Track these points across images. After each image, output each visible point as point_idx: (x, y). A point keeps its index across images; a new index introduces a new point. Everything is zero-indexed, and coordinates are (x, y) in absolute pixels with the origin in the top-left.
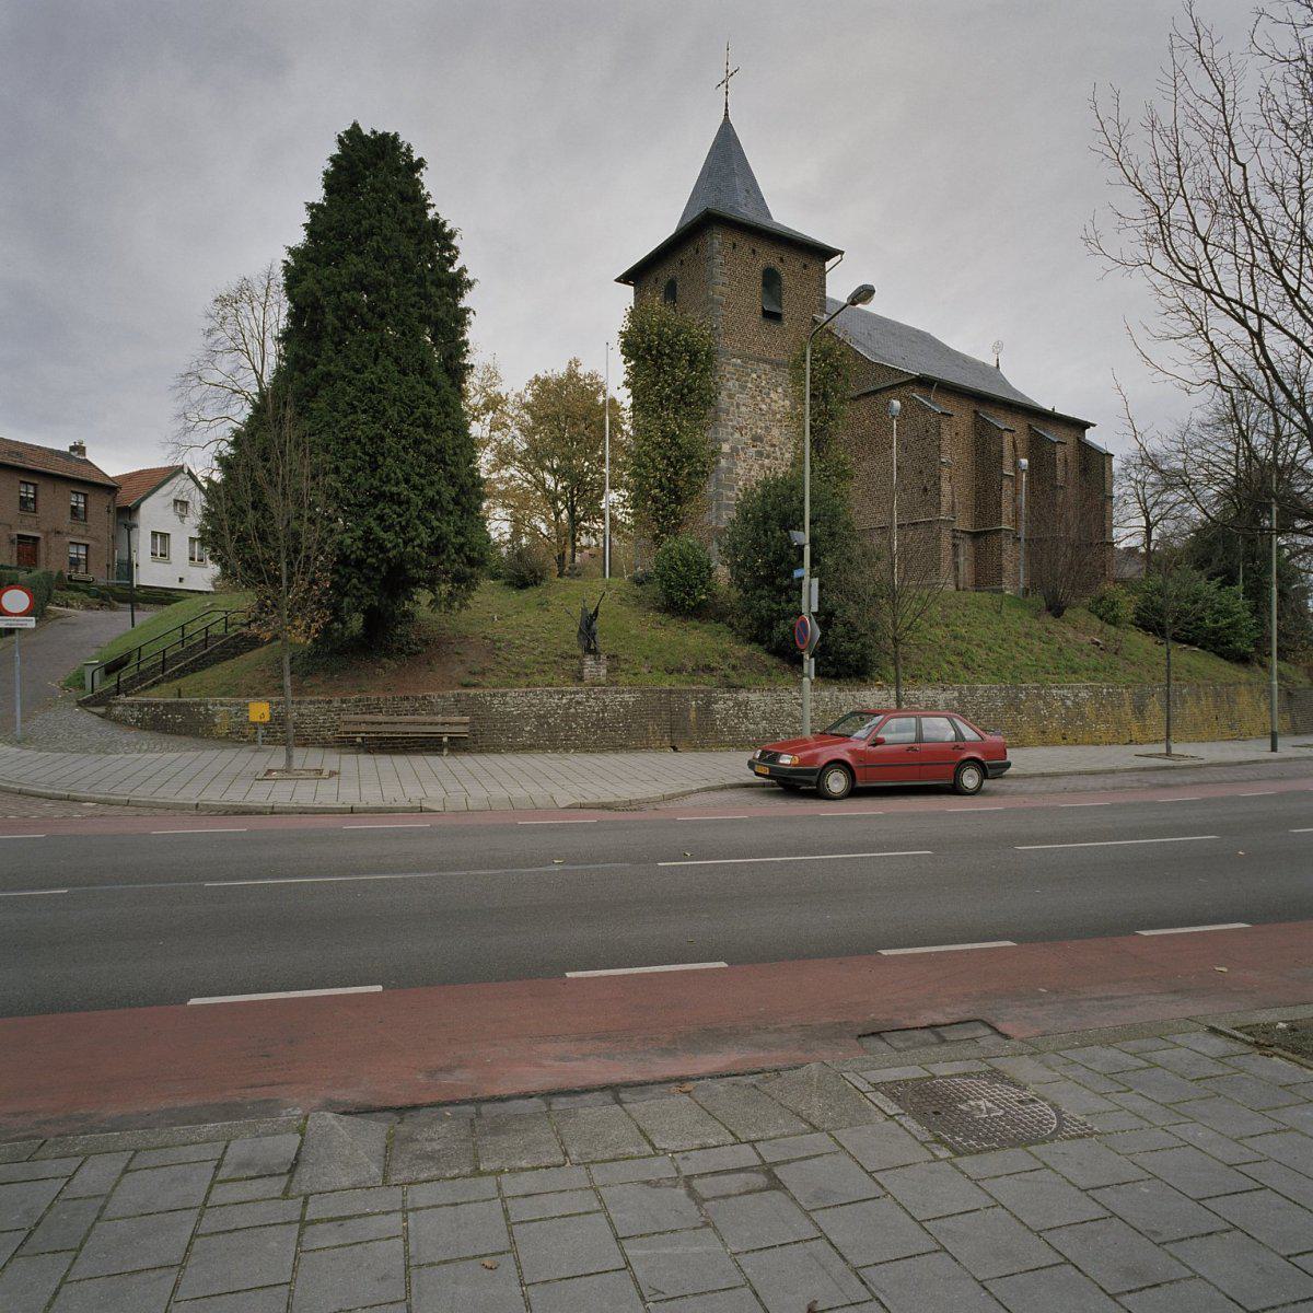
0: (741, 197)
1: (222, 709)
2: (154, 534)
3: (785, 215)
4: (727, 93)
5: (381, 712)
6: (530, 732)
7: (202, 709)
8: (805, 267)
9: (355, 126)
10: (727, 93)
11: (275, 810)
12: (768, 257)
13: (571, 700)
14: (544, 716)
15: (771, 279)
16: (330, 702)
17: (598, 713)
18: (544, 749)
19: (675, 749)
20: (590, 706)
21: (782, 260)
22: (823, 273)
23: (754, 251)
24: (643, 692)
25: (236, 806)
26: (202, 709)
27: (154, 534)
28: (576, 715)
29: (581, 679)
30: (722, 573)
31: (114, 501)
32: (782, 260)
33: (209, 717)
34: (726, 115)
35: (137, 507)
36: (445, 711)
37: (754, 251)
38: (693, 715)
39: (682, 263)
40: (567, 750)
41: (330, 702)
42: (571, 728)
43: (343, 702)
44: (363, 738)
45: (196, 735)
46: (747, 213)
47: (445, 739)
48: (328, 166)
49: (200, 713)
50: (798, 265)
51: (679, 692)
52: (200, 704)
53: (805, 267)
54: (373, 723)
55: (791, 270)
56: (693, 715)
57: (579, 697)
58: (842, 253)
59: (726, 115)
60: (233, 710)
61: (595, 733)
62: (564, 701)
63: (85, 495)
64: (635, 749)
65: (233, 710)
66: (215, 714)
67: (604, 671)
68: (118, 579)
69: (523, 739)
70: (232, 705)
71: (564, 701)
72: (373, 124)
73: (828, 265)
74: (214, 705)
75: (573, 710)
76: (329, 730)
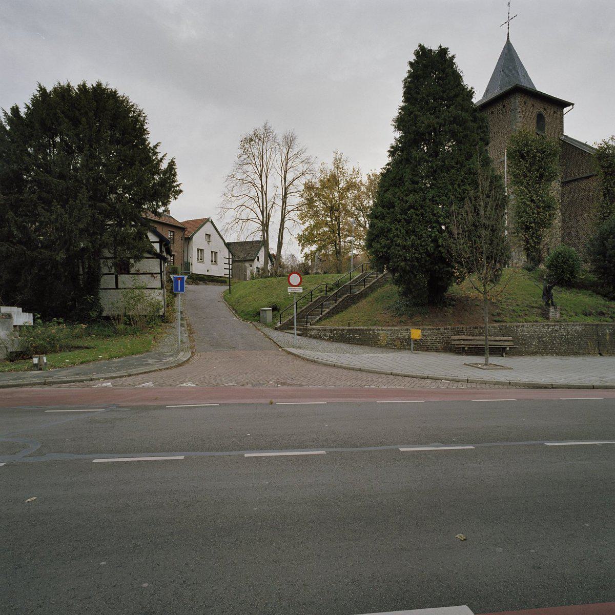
0: (522, 78)
1: (382, 332)
2: (198, 250)
3: (542, 86)
4: (508, 28)
5: (464, 334)
6: (535, 345)
7: (371, 332)
8: (555, 112)
9: (448, 48)
10: (508, 28)
11: (554, 386)
12: (539, 108)
13: (553, 329)
14: (541, 337)
15: (540, 118)
16: (439, 329)
17: (565, 336)
18: (542, 354)
19: (601, 355)
20: (561, 332)
21: (545, 109)
22: (562, 114)
23: (533, 105)
24: (585, 325)
25: (534, 384)
26: (371, 332)
27: (198, 250)
28: (555, 337)
29: (548, 319)
30: (587, 267)
31: (184, 234)
32: (545, 109)
33: (375, 336)
34: (508, 39)
35: (192, 237)
36: (495, 335)
37: (533, 105)
38: (608, 337)
39: (492, 113)
40: (552, 354)
41: (439, 329)
42: (553, 343)
43: (445, 329)
44: (468, 348)
45: (369, 345)
46: (525, 84)
47: (508, 349)
48: (75, 85)
49: (371, 334)
50: (552, 112)
51: (601, 325)
52: (370, 330)
53: (555, 112)
54: (466, 340)
55: (548, 113)
56: (608, 337)
57: (557, 328)
58: (573, 104)
59: (508, 39)
60: (389, 333)
61: (564, 346)
62: (550, 330)
63: (173, 232)
64: (583, 354)
65: (389, 333)
66: (379, 335)
67: (558, 315)
68: (185, 270)
69: (532, 349)
70: (388, 330)
71: (550, 330)
72: (433, 46)
73: (565, 110)
74: (379, 330)
75: (554, 334)
76: (439, 343)
